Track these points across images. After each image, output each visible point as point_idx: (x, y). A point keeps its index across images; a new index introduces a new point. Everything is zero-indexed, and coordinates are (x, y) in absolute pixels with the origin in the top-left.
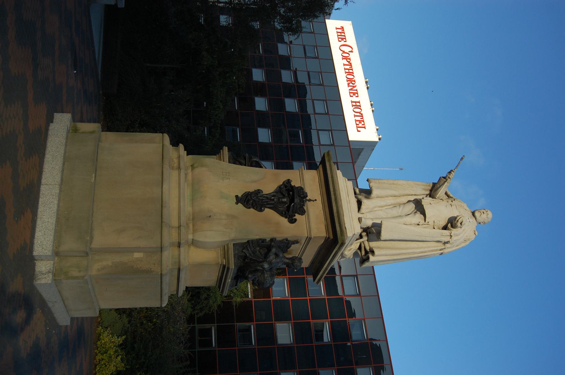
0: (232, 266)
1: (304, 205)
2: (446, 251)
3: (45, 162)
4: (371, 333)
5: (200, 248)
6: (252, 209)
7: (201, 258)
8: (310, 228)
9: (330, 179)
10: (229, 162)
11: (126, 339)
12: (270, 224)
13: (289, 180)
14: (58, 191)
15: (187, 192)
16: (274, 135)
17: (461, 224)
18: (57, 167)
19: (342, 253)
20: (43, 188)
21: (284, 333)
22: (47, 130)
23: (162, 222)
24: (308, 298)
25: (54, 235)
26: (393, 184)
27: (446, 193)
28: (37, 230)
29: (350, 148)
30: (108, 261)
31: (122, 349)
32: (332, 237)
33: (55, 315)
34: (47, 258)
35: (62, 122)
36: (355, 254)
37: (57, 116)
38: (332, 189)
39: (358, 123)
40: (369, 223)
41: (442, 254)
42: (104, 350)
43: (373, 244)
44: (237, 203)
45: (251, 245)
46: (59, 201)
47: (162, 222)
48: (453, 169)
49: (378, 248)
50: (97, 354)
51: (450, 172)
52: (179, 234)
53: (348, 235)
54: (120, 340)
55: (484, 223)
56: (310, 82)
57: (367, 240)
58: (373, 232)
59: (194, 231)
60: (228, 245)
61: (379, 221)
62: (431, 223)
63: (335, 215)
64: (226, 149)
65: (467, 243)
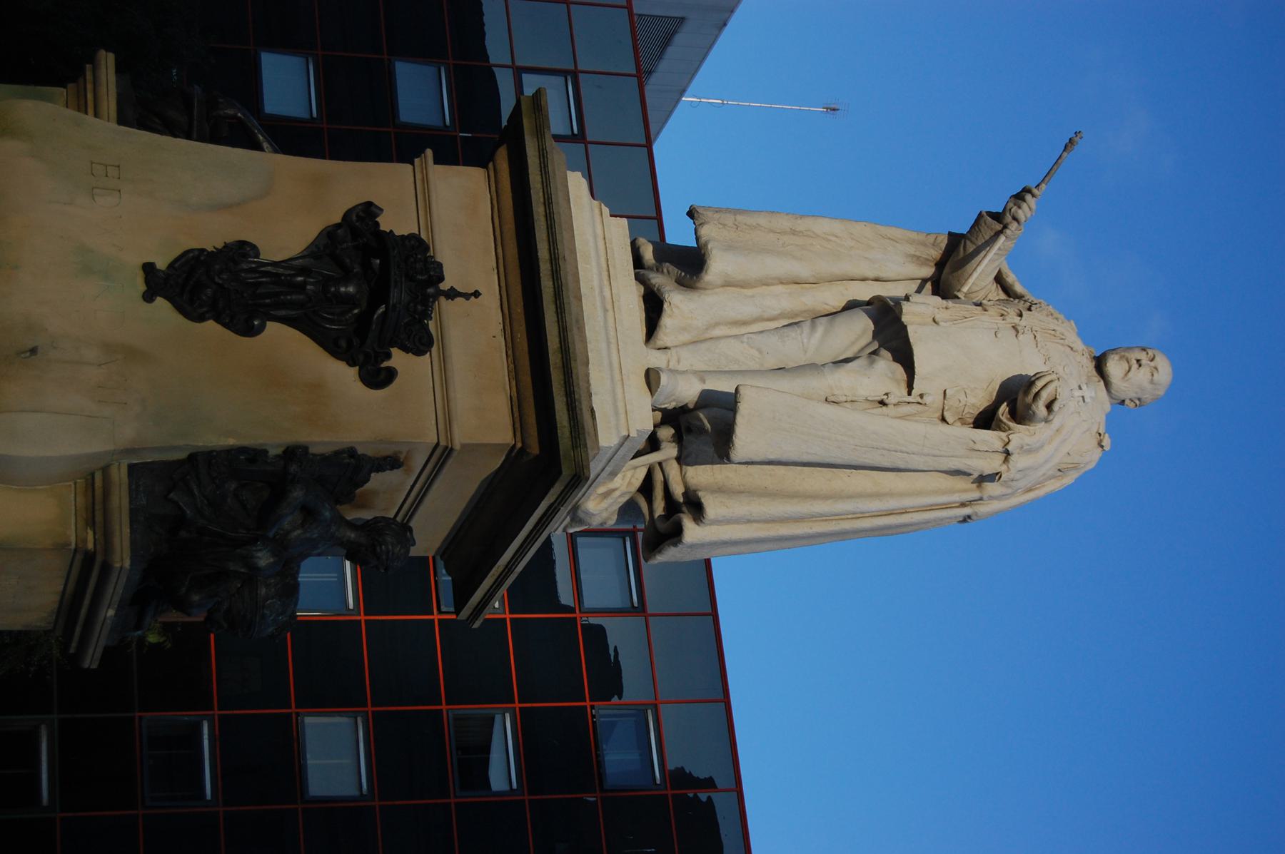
0: (122, 558)
2: (983, 509)
4: (676, 744)
6: (211, 325)
9: (539, 210)
10: (122, 121)
12: (289, 389)
13: (370, 204)
17: (1049, 407)
19: (576, 508)
21: (335, 755)
24: (436, 617)
27: (999, 279)
29: (631, 14)
32: (535, 449)
36: (629, 509)
40: (686, 391)
41: (966, 519)
43: (700, 475)
44: (148, 297)
48: (1032, 185)
49: (720, 490)
51: (1019, 197)
58: (702, 427)
60: (105, 470)
63: (554, 359)
64: (107, 60)
65: (1069, 480)
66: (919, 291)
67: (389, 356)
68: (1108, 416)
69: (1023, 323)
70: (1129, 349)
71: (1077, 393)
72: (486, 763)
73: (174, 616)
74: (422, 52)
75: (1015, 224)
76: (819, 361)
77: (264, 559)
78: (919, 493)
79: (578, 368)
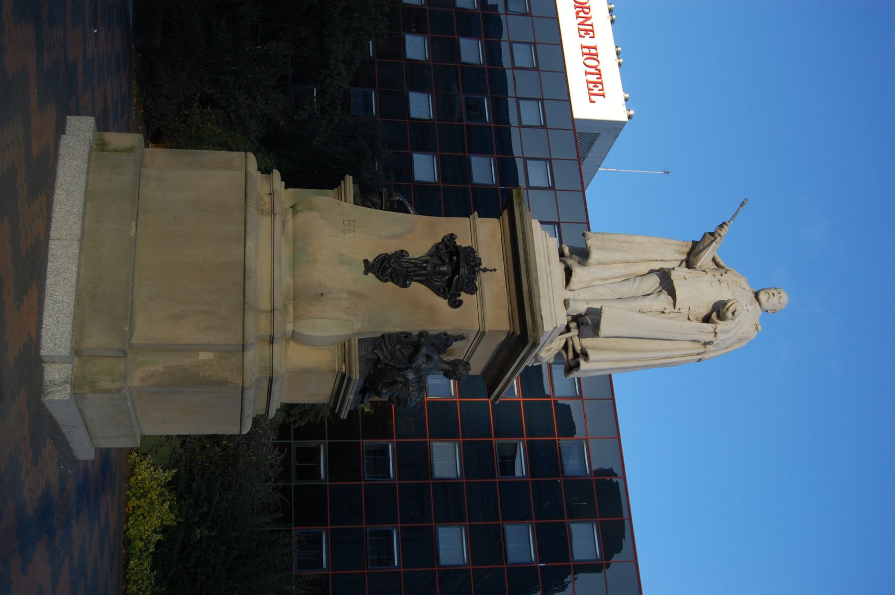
0: (356, 376)
1: (474, 279)
3: (55, 202)
4: (597, 459)
5: (304, 345)
7: (308, 360)
8: (483, 312)
10: (355, 203)
11: (177, 475)
12: (419, 309)
13: (452, 234)
14: (77, 251)
15: (285, 252)
16: (438, 107)
17: (733, 314)
18: (75, 211)
19: (536, 355)
20: (53, 245)
21: (446, 459)
22: (57, 147)
23: (244, 304)
25: (73, 323)
26: (627, 242)
27: (714, 260)
28: (46, 314)
30: (159, 365)
31: (171, 491)
32: (518, 332)
33: (72, 445)
34: (62, 360)
35: (80, 131)
36: (558, 356)
37: (73, 121)
38: (521, 253)
39: (591, 86)
40: (582, 308)
41: (700, 360)
42: (141, 491)
43: (588, 342)
44: (366, 273)
45: (387, 341)
46: (79, 267)
47: (244, 304)
48: (727, 221)
49: (595, 348)
50: (129, 499)
51: (721, 226)
52: (272, 323)
53: (546, 329)
54: (168, 475)
55: (775, 311)
56: (506, 8)
57: (578, 335)
58: (587, 322)
59: (296, 318)
60: (349, 341)
61: (597, 306)
62: (684, 310)
64: (349, 179)
65: (744, 344)
66: (679, 266)
67: (460, 295)
68: (761, 317)
69: (723, 278)
70: (769, 289)
71: (746, 308)
72: (513, 464)
73: (376, 398)
74: (484, 151)
75: (719, 238)
76: (637, 295)
77: (411, 376)
78: (679, 350)
79: (535, 300)
